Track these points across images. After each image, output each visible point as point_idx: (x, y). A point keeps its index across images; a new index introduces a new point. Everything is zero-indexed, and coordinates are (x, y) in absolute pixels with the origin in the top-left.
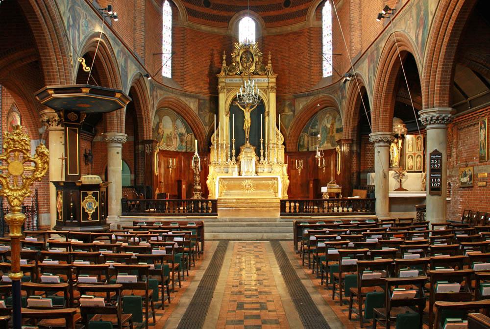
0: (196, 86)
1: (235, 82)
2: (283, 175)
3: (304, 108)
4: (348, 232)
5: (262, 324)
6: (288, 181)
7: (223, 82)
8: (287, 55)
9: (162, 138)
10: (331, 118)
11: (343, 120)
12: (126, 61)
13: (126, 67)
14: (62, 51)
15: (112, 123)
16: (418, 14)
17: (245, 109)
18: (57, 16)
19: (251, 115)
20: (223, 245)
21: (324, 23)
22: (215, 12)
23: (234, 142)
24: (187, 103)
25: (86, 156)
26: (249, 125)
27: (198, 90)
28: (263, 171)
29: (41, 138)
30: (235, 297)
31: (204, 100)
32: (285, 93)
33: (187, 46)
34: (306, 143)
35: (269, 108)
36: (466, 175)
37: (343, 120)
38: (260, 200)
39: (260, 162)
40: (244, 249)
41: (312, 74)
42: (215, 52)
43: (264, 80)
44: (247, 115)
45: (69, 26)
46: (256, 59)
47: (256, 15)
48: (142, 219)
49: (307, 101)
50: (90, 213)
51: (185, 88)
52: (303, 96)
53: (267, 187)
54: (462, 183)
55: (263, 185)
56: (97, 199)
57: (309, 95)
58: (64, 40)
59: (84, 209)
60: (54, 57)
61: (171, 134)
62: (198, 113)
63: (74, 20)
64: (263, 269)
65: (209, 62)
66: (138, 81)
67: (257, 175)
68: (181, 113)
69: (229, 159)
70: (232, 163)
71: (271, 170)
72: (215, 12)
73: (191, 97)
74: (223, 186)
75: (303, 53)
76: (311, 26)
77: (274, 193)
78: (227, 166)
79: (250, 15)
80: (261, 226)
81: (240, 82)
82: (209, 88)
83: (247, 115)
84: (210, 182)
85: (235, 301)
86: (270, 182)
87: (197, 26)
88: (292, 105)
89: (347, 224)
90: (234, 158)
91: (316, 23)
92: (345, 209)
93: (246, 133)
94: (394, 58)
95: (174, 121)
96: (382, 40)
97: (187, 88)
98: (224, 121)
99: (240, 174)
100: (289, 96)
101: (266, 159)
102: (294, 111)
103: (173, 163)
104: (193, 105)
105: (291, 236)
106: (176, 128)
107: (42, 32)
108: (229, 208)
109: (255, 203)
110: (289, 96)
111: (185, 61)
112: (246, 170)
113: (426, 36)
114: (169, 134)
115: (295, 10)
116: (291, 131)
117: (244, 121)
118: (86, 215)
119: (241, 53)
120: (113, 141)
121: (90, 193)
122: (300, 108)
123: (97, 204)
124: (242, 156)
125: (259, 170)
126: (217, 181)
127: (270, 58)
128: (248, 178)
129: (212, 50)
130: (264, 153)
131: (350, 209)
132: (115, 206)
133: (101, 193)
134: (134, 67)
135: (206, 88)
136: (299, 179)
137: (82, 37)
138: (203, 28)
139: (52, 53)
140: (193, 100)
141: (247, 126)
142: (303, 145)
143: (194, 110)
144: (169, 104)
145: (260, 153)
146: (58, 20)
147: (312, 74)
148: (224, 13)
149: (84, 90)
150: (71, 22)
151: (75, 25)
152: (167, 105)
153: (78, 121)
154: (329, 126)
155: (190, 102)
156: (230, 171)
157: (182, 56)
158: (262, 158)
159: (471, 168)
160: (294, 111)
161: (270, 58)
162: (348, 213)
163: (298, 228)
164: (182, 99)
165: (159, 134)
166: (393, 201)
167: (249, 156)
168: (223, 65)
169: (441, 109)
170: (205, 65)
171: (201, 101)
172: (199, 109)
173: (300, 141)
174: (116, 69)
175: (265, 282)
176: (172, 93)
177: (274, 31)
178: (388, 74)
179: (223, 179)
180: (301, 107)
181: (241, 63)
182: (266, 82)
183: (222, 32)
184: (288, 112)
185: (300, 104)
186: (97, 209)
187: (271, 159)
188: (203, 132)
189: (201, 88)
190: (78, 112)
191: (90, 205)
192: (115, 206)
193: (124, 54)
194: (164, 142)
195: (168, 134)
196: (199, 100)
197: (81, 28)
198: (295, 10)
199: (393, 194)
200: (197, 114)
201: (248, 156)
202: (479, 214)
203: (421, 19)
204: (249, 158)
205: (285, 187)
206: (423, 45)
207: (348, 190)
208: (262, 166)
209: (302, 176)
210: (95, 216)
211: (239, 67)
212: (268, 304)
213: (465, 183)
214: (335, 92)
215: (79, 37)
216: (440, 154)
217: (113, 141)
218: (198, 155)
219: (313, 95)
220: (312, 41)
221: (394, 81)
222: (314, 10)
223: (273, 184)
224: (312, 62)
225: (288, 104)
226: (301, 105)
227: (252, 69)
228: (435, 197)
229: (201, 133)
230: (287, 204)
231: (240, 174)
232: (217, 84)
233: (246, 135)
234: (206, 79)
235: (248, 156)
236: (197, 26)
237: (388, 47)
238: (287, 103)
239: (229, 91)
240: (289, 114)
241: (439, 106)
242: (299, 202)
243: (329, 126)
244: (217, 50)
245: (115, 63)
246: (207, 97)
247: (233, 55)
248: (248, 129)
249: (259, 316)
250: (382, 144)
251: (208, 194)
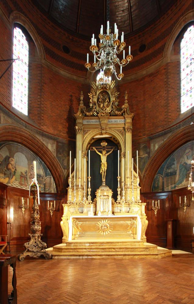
1: (92, 123)
2: (142, 215)
3: (160, 148)
6: (147, 222)
7: (80, 123)
8: (142, 99)
9: (14, 175)
17: (101, 153)
19: (107, 158)
21: (182, 56)
23: (89, 180)
24: (44, 142)
26: (106, 169)
27: (56, 132)
28: (121, 210)
31: (62, 143)
32: (140, 136)
33: (45, 85)
34: (160, 184)
35: (125, 149)
38: (120, 244)
39: (117, 201)
41: (170, 111)
42: (74, 98)
43: (120, 121)
44: (104, 159)
46: (113, 99)
49: (163, 140)
51: (42, 127)
52: (159, 136)
53: (126, 228)
55: (121, 226)
57: (166, 134)
61: (26, 173)
62: (57, 155)
65: (68, 107)
67: (114, 215)
69: (85, 199)
70: (87, 202)
71: (129, 209)
74: (77, 227)
75: (159, 92)
76: (169, 61)
77: (132, 235)
78: (81, 205)
81: (97, 123)
82: (68, 133)
83: (104, 159)
84: (64, 223)
86: (129, 222)
88: (147, 147)
90: (89, 197)
91: (174, 58)
93: (103, 176)
97: (45, 128)
99: (95, 214)
100: (145, 138)
101: (123, 198)
102: (149, 153)
103: (26, 202)
104: (51, 147)
108: (78, 257)
109: (114, 248)
111: (42, 99)
112: (102, 210)
114: (24, 173)
115: (150, 52)
116: (146, 173)
117: (100, 165)
119: (98, 93)
122: (156, 149)
124: (99, 193)
125: (116, 210)
126: (71, 221)
127: (126, 98)
128: (105, 218)
129: (71, 96)
130: (121, 192)
135: (65, 132)
136: (155, 220)
138: (63, 72)
140: (51, 141)
141: (103, 169)
142: (158, 186)
143: (52, 151)
144: (22, 139)
145: (117, 192)
147: (170, 111)
152: (19, 140)
155: (48, 143)
156: (85, 210)
157: (39, 94)
158: (119, 197)
160: (149, 153)
161: (126, 98)
164: (39, 138)
165: (9, 169)
167: (105, 194)
168: (80, 105)
170: (64, 110)
171: (60, 144)
173: (154, 184)
176: (26, 127)
179: (77, 219)
180: (157, 147)
181: (98, 104)
182: (122, 123)
183: (81, 80)
185: (156, 145)
187: (128, 198)
188: (61, 174)
189: (60, 131)
194: (16, 180)
195: (21, 173)
196: (58, 142)
198: (150, 52)
200: (55, 156)
201: (104, 193)
204: (105, 197)
205: (144, 228)
208: (119, 205)
209: (158, 218)
211: (96, 108)
218: (36, 182)
219: (171, 132)
220: (169, 77)
222: (173, 42)
223: (132, 225)
224: (170, 98)
225: (144, 147)
226: (156, 146)
227: (109, 110)
229: (60, 176)
231: (95, 214)
232: (75, 125)
233: (103, 178)
234: (64, 124)
235: (104, 193)
238: (142, 146)
239: (85, 132)
240: (143, 156)
244: (75, 97)
246: (65, 141)
247: (90, 95)
248: (104, 173)
251: (62, 236)
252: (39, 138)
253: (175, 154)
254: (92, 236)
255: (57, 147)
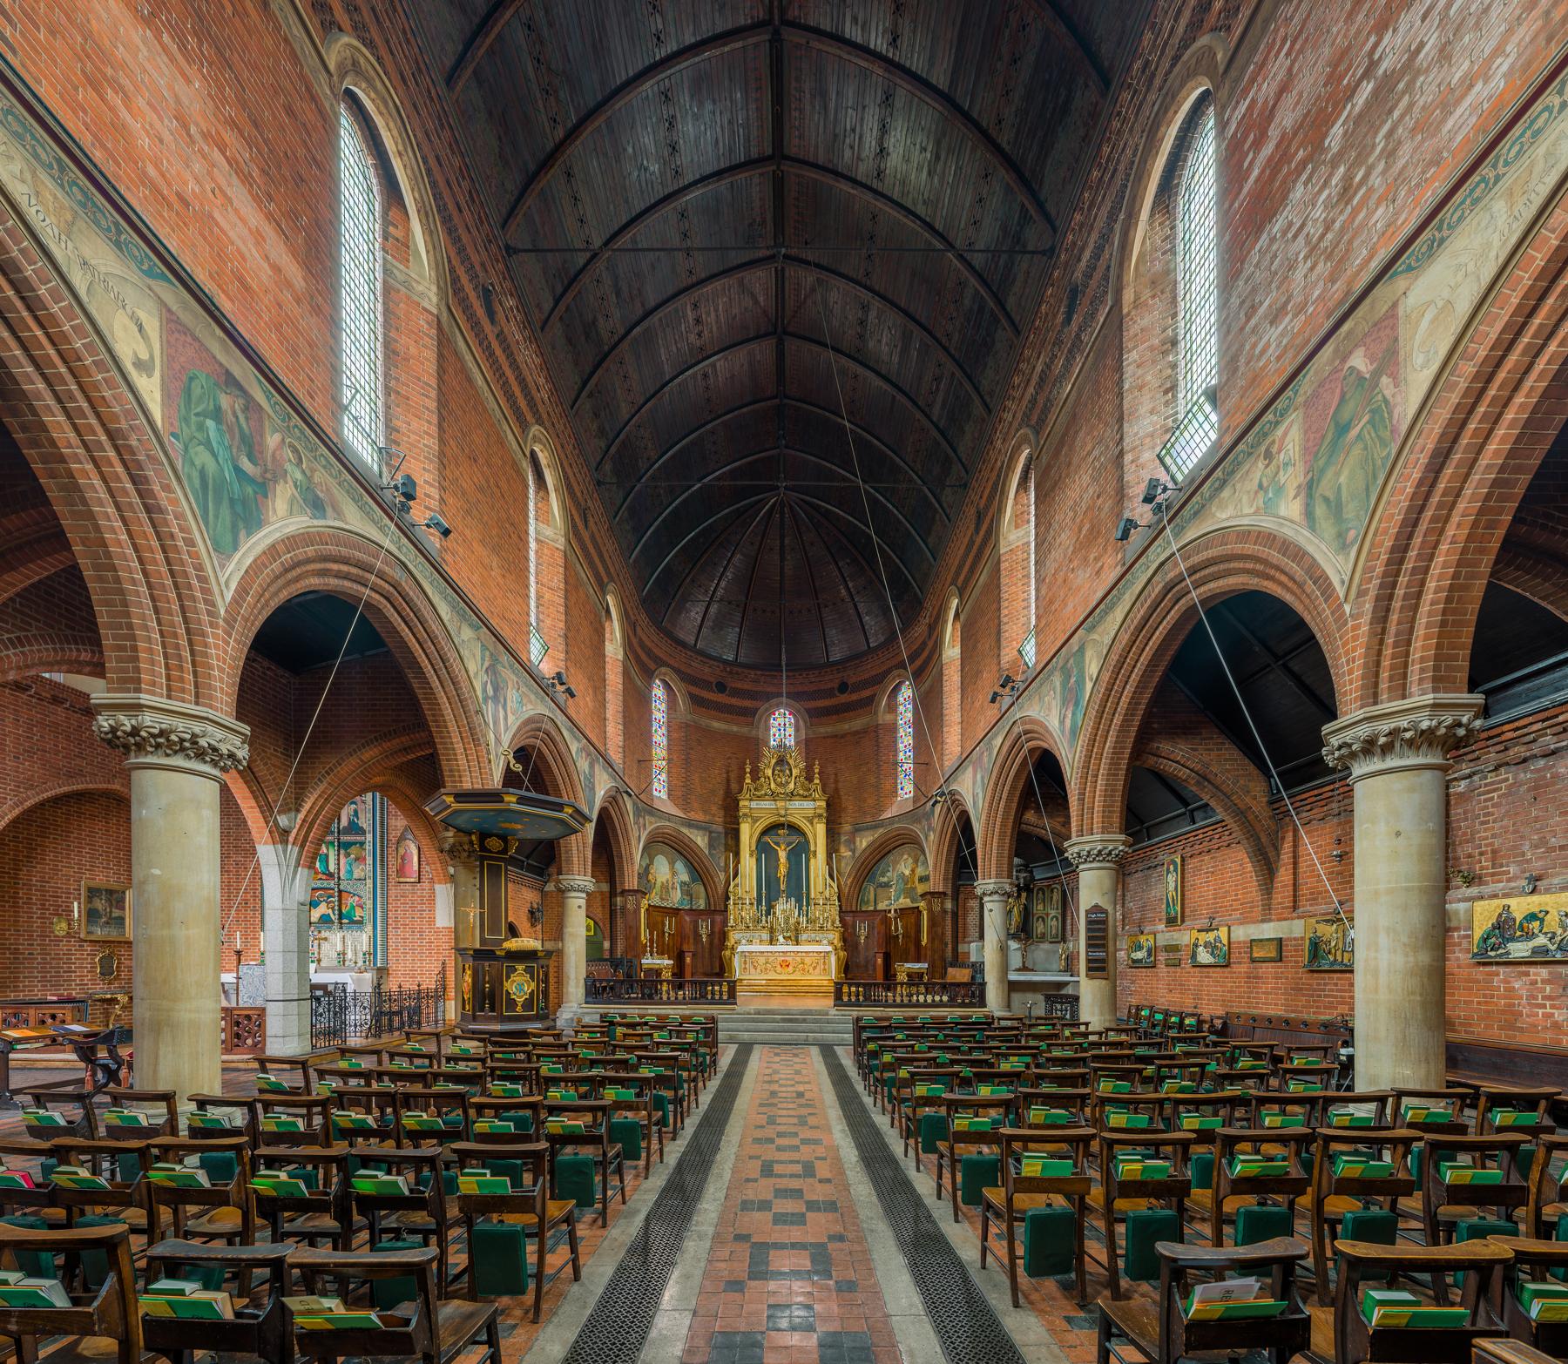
0: (705, 812)
4: (941, 1037)
5: (803, 1215)
10: (910, 861)
11: (931, 862)
12: (592, 766)
13: (592, 775)
14: (474, 737)
15: (569, 861)
16: (1065, 683)
18: (462, 677)
20: (745, 1049)
22: (734, 701)
25: (532, 913)
29: (285, 842)
30: (756, 1149)
36: (1140, 948)
37: (931, 862)
40: (777, 1059)
44: (782, 855)
45: (486, 699)
46: (795, 772)
47: (797, 705)
48: (614, 1010)
50: (520, 1001)
52: (867, 829)
54: (1134, 961)
56: (532, 978)
57: (876, 827)
58: (477, 720)
59: (508, 993)
60: (459, 747)
63: (496, 689)
64: (807, 1095)
66: (613, 799)
68: (679, 848)
72: (734, 701)
73: (698, 828)
79: (787, 706)
80: (804, 1021)
83: (782, 855)
85: (758, 1157)
87: (704, 722)
89: (940, 1024)
91: (889, 717)
92: (937, 998)
94: (1018, 760)
95: (672, 863)
96: (996, 735)
98: (748, 864)
102: (853, 851)
104: (701, 840)
105: (849, 1037)
106: (674, 873)
107: (435, 704)
110: (847, 828)
113: (1080, 717)
115: (855, 697)
118: (512, 1004)
120: (573, 889)
121: (520, 967)
123: (533, 985)
131: (945, 998)
132: (575, 989)
133: (543, 964)
134: (605, 776)
137: (511, 718)
138: (716, 725)
139: (456, 739)
146: (464, 685)
148: (747, 703)
149: (514, 799)
150: (490, 692)
151: (498, 695)
153: (505, 851)
154: (907, 872)
159: (1151, 938)
160: (853, 851)
162: (941, 1005)
163: (859, 1027)
164: (685, 830)
166: (1013, 987)
169: (1106, 837)
172: (711, 846)
174: (575, 777)
175: (811, 1121)
177: (822, 730)
178: (1007, 788)
180: (864, 844)
183: (745, 730)
184: (845, 852)
186: (532, 993)
190: (503, 838)
191: (519, 986)
192: (575, 989)
193: (589, 754)
197: (509, 704)
198: (855, 697)
199: (1013, 977)
202: (1167, 1014)
203: (1070, 690)
206: (1074, 733)
207: (938, 968)
210: (528, 1004)
212: (818, 1164)
213: (1139, 961)
214: (918, 821)
215: (506, 718)
216: (1105, 912)
217: (573, 889)
221: (1016, 799)
226: (863, 842)
228: (1097, 982)
230: (845, 989)
236: (704, 722)
237: (1008, 744)
238: (843, 838)
239: (755, 820)
241: (1435, 690)
242: (864, 985)
243: (907, 872)
245: (572, 768)
247: (761, 766)
249: (800, 1191)
250: (996, 897)
252: (685, 830)
253: (891, 857)
254: (1185, 99)
255: (710, 839)
